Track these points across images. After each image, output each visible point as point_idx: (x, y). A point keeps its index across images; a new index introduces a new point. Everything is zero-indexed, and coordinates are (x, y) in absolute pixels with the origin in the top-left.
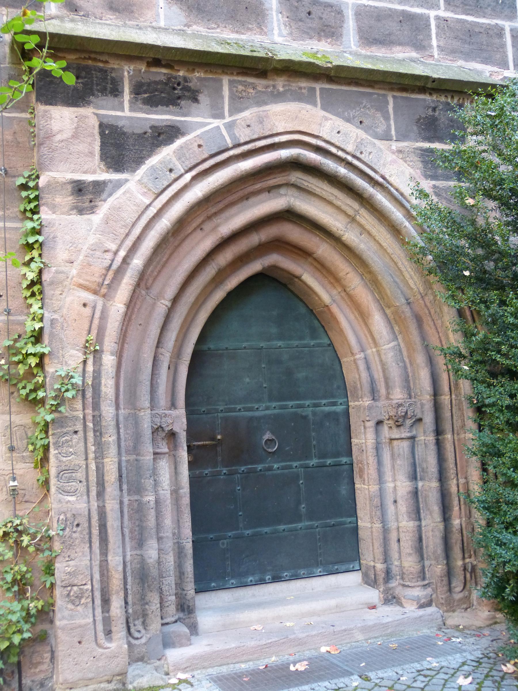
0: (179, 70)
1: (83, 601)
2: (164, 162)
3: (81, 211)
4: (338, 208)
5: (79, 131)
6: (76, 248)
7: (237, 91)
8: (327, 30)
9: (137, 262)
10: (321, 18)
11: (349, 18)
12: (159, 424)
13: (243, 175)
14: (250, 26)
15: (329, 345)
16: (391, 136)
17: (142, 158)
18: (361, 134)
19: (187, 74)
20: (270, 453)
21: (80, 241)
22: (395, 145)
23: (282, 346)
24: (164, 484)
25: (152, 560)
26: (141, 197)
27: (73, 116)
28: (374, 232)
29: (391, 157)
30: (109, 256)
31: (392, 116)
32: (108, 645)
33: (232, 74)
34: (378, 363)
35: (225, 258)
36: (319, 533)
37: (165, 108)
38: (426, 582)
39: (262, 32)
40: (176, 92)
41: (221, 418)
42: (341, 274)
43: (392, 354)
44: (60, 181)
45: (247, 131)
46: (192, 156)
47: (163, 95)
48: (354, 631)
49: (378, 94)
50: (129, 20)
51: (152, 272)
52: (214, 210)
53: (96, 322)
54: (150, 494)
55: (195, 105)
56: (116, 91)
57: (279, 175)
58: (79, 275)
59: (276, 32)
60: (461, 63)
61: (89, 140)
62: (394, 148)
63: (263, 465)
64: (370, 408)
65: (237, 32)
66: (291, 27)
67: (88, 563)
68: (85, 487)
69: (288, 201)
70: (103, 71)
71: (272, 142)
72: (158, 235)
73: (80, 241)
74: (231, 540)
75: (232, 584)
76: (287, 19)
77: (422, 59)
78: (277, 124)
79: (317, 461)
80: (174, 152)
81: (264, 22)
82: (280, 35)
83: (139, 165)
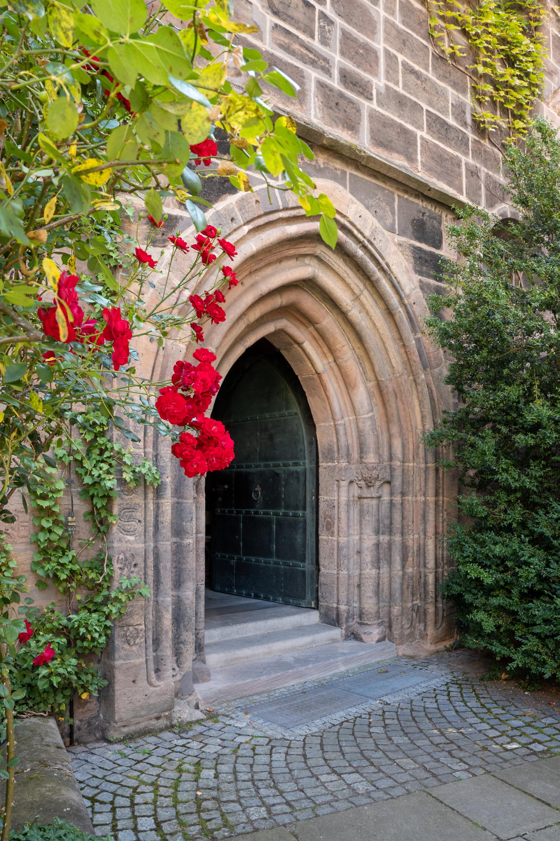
1: (138, 641)
10: (345, 111)
22: (398, 239)
25: (189, 601)
29: (394, 248)
32: (158, 683)
42: (338, 346)
64: (346, 469)
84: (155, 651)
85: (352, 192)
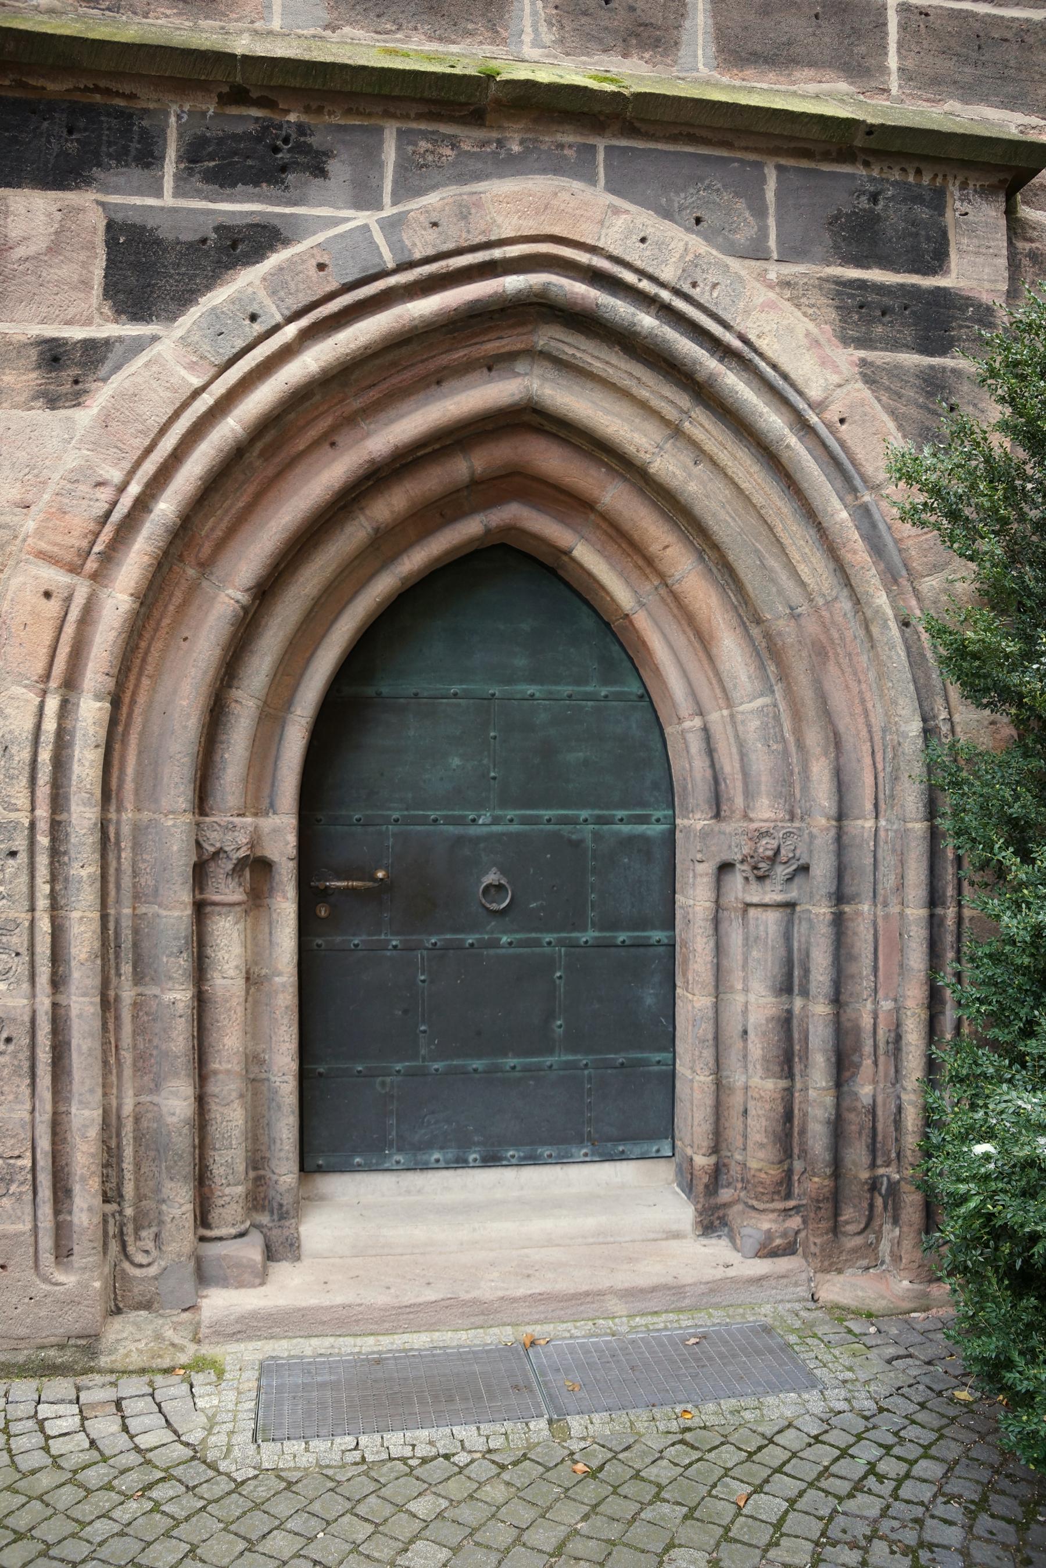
0: (287, 112)
2: (240, 300)
3: (53, 402)
4: (643, 405)
5: (64, 239)
6: (37, 476)
7: (414, 152)
8: (645, 34)
9: (167, 507)
11: (696, 9)
12: (218, 845)
13: (416, 327)
14: (470, 26)
15: (641, 697)
16: (767, 250)
17: (192, 292)
18: (697, 244)
19: (304, 118)
20: (496, 912)
21: (47, 463)
22: (774, 271)
23: (537, 695)
24: (226, 967)
25: (175, 1119)
26: (183, 372)
27: (54, 209)
28: (723, 457)
29: (763, 295)
30: (105, 495)
31: (772, 210)
32: (61, 1277)
33: (406, 117)
34: (732, 740)
35: (388, 506)
36: (590, 1078)
37: (250, 189)
38: (791, 1203)
39: (496, 37)
40: (280, 156)
41: (394, 835)
42: (654, 548)
43: (758, 723)
44: (14, 341)
45: (431, 235)
46: (302, 286)
47: (249, 162)
48: (607, 1297)
49: (740, 161)
50: (206, 18)
51: (212, 529)
52: (357, 404)
53: (69, 630)
54: (177, 986)
55: (319, 181)
56: (148, 157)
57: (509, 332)
58: (39, 533)
59: (527, 38)
60: (953, 105)
61: (83, 256)
62: (772, 276)
63: (477, 936)
65: (440, 39)
66: (562, 27)
67: (27, 1117)
68: (27, 966)
69: (527, 387)
70: (125, 116)
71: (487, 258)
72: (213, 452)
73: (47, 463)
74: (400, 1078)
75: (398, 1162)
76: (554, 12)
77: (861, 97)
78: (499, 220)
79: (597, 934)
80: (264, 279)
81: (501, 18)
82: (536, 43)
83: (184, 305)
84: (57, 1212)
85: (612, 188)
